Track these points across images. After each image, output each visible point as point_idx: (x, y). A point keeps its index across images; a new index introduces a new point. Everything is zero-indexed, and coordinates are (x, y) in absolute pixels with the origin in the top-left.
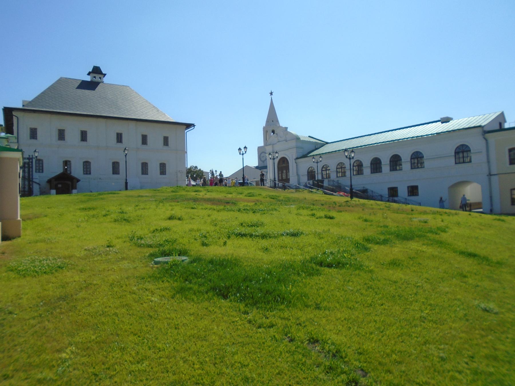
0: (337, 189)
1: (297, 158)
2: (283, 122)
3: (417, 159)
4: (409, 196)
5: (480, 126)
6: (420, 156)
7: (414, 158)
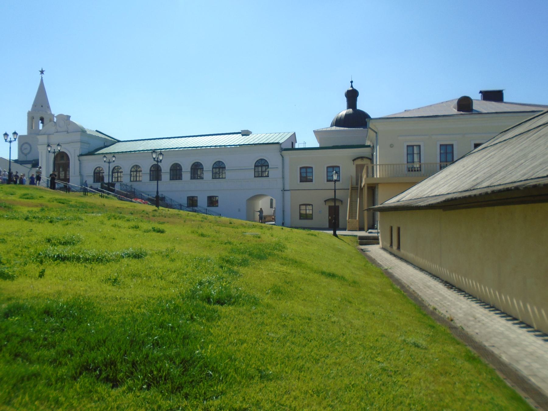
0: (130, 195)
1: (81, 155)
2: (57, 108)
3: (219, 168)
4: (208, 206)
5: (278, 143)
6: (222, 166)
7: (216, 168)
